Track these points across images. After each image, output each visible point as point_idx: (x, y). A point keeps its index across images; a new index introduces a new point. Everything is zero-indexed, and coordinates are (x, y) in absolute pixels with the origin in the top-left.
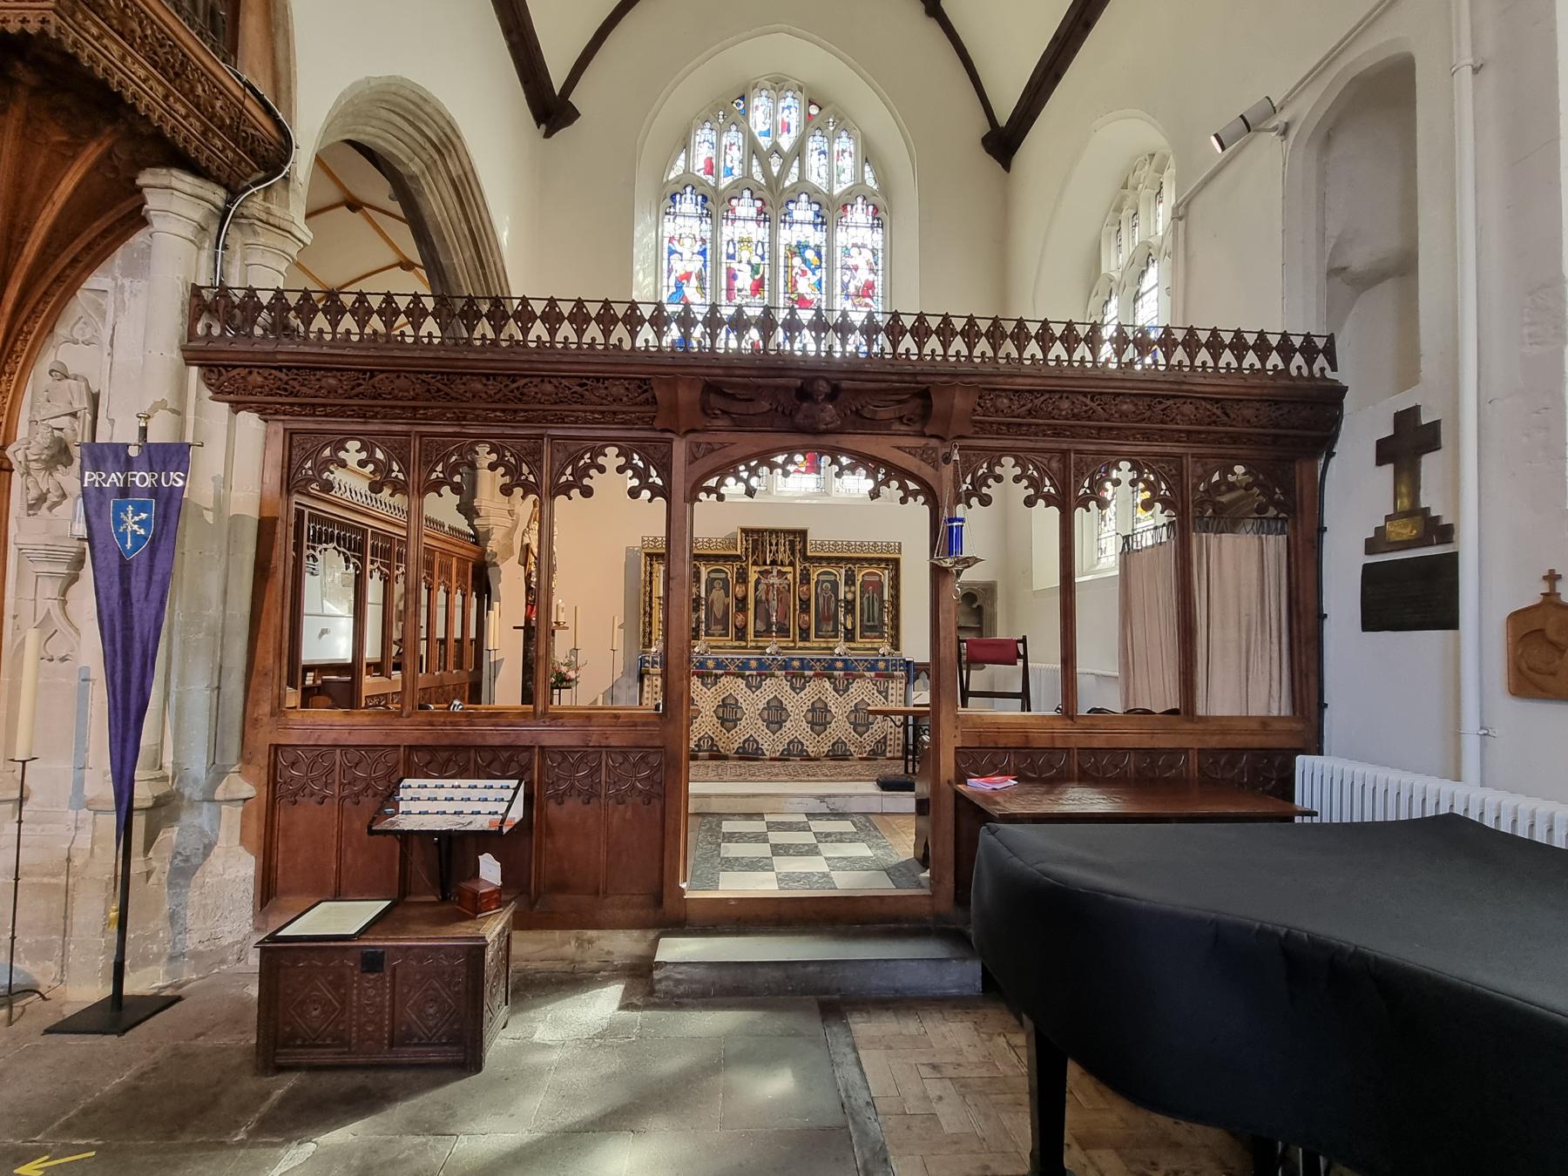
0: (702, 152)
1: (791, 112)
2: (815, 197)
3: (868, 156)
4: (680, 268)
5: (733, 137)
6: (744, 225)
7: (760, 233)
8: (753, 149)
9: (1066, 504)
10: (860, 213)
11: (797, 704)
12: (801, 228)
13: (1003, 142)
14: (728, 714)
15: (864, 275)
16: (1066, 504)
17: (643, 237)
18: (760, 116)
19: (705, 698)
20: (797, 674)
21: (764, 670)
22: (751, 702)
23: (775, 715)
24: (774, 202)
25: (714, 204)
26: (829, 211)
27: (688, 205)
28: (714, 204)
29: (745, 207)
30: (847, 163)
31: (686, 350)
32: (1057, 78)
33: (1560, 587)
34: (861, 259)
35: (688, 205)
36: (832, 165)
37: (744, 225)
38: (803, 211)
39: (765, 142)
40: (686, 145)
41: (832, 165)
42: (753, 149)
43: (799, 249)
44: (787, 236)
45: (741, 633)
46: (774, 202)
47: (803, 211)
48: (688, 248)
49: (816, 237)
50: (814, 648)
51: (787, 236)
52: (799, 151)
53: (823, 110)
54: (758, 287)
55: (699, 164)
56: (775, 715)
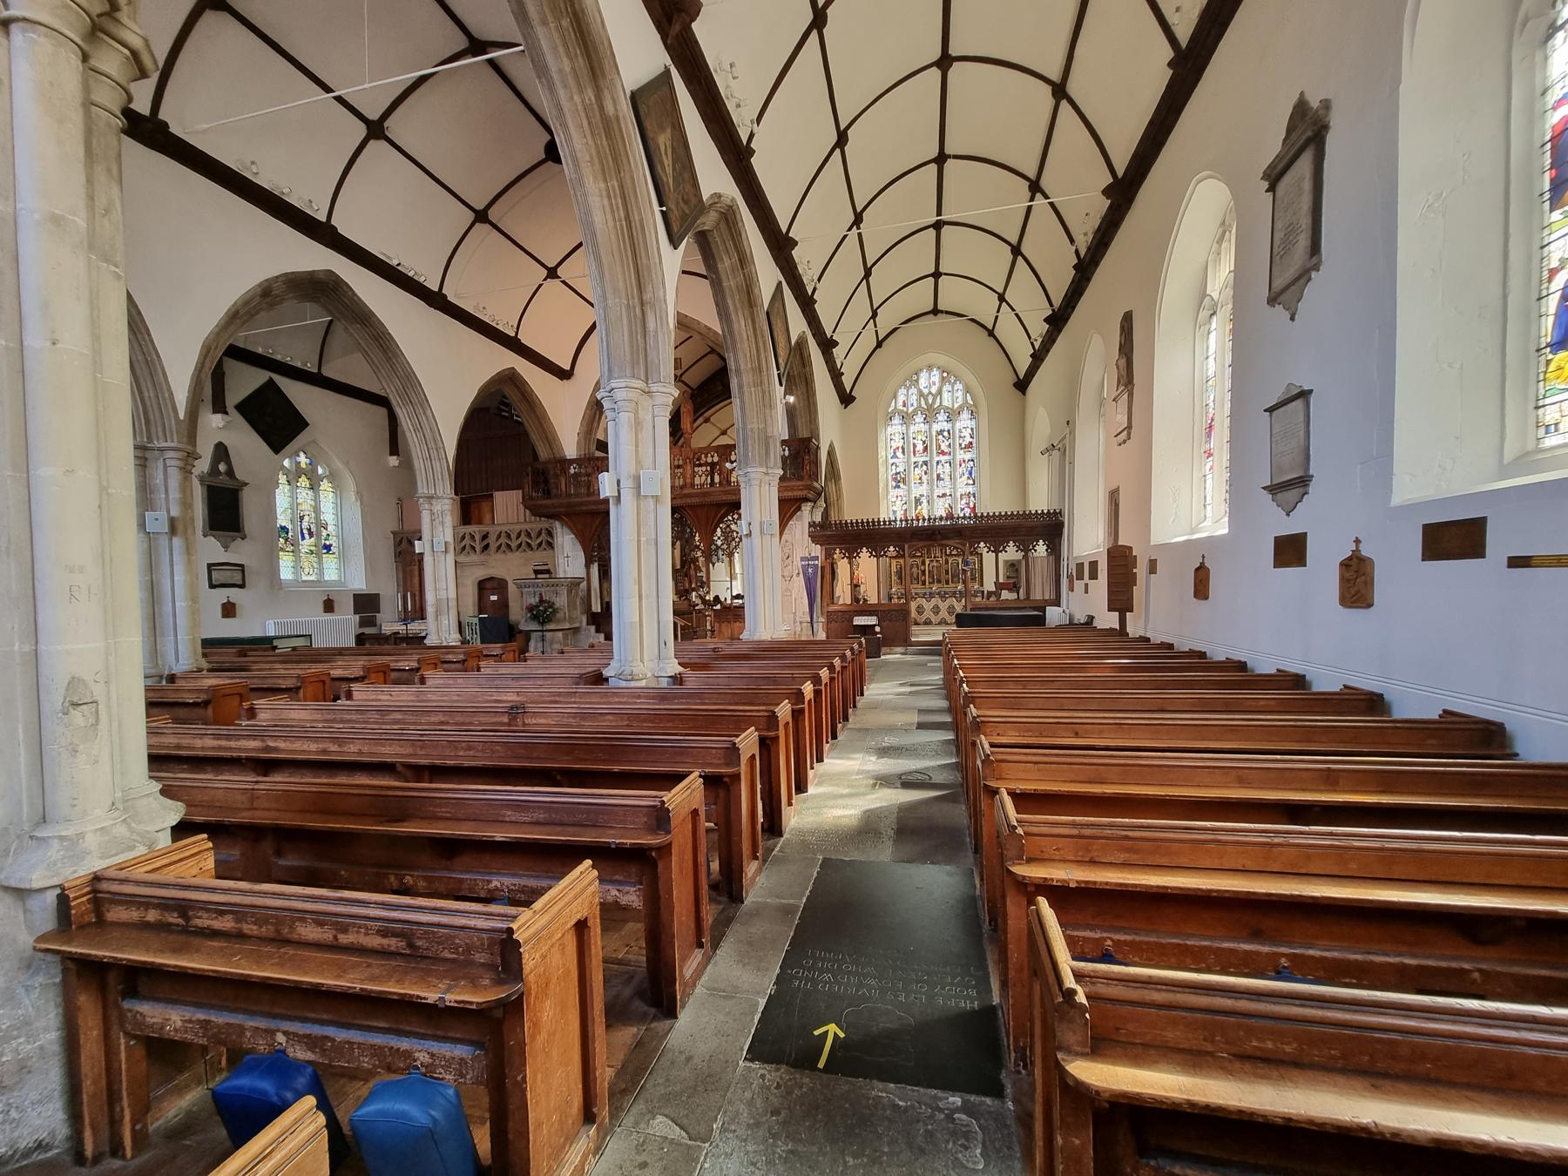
0: (901, 398)
1: (936, 376)
2: (947, 410)
3: (967, 390)
4: (895, 445)
5: (913, 390)
6: (918, 425)
7: (923, 427)
8: (921, 394)
9: (997, 552)
10: (965, 415)
11: (944, 606)
12: (941, 424)
13: (1022, 385)
14: (920, 610)
15: (968, 439)
16: (997, 552)
17: (881, 438)
18: (923, 382)
19: (913, 605)
20: (943, 597)
21: (932, 595)
22: (928, 606)
23: (936, 610)
24: (930, 414)
25: (907, 418)
26: (952, 415)
27: (897, 420)
28: (907, 418)
29: (919, 418)
30: (960, 394)
31: (1060, 1048)
32: (1081, 294)
33: (1361, 547)
34: (966, 433)
35: (897, 420)
36: (953, 396)
37: (918, 425)
38: (942, 417)
39: (926, 391)
40: (895, 397)
41: (953, 396)
42: (921, 394)
43: (940, 433)
44: (936, 427)
45: (924, 583)
46: (930, 414)
47: (942, 417)
48: (897, 438)
49: (946, 426)
50: (951, 587)
51: (936, 427)
52: (940, 392)
53: (947, 375)
54: (925, 449)
55: (900, 403)
56: (936, 610)
